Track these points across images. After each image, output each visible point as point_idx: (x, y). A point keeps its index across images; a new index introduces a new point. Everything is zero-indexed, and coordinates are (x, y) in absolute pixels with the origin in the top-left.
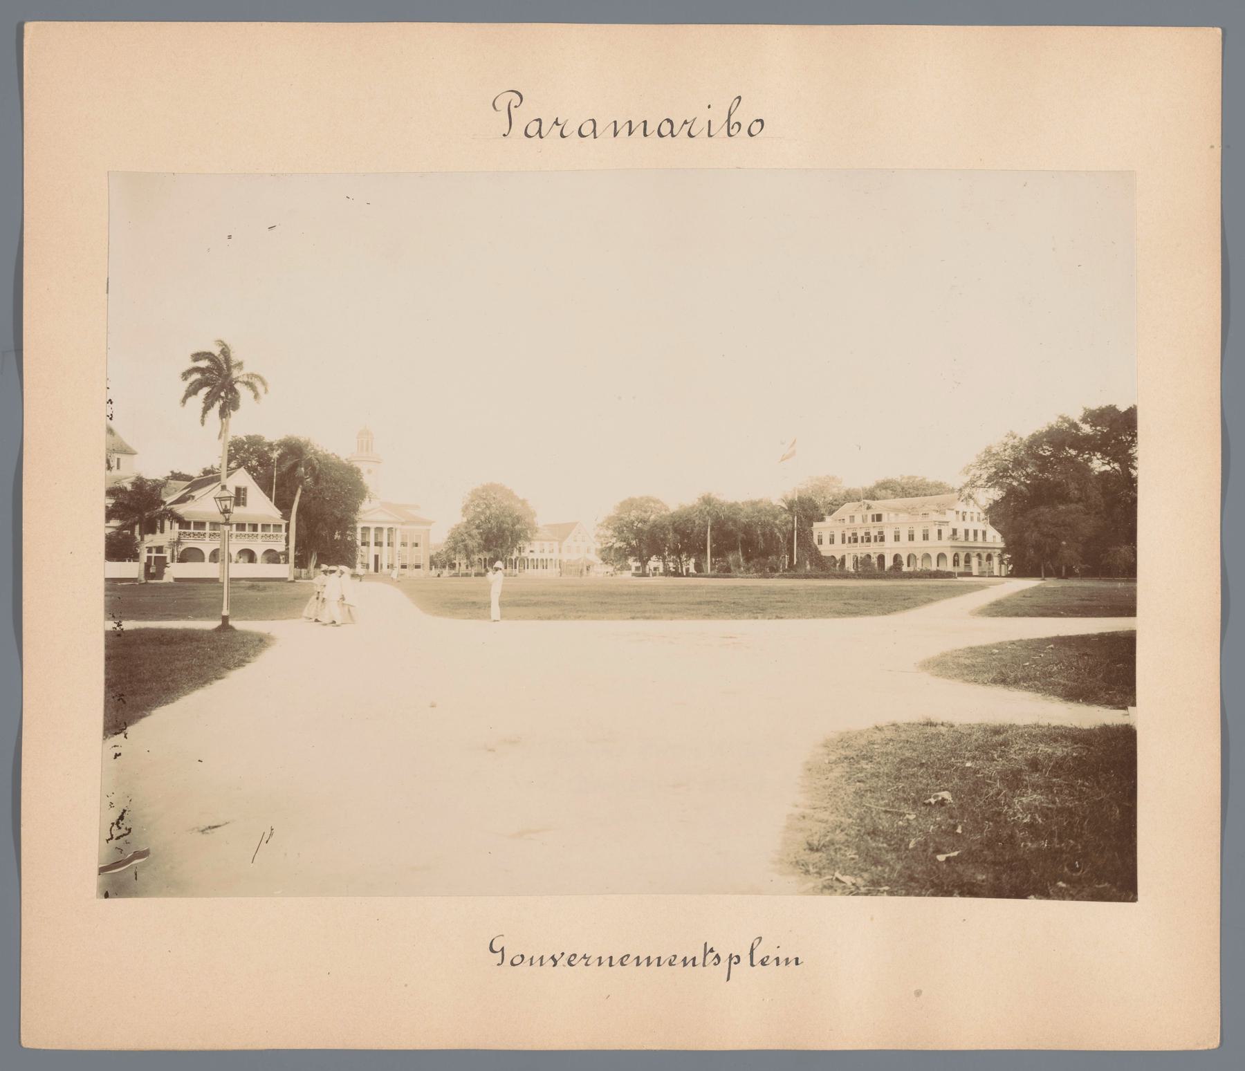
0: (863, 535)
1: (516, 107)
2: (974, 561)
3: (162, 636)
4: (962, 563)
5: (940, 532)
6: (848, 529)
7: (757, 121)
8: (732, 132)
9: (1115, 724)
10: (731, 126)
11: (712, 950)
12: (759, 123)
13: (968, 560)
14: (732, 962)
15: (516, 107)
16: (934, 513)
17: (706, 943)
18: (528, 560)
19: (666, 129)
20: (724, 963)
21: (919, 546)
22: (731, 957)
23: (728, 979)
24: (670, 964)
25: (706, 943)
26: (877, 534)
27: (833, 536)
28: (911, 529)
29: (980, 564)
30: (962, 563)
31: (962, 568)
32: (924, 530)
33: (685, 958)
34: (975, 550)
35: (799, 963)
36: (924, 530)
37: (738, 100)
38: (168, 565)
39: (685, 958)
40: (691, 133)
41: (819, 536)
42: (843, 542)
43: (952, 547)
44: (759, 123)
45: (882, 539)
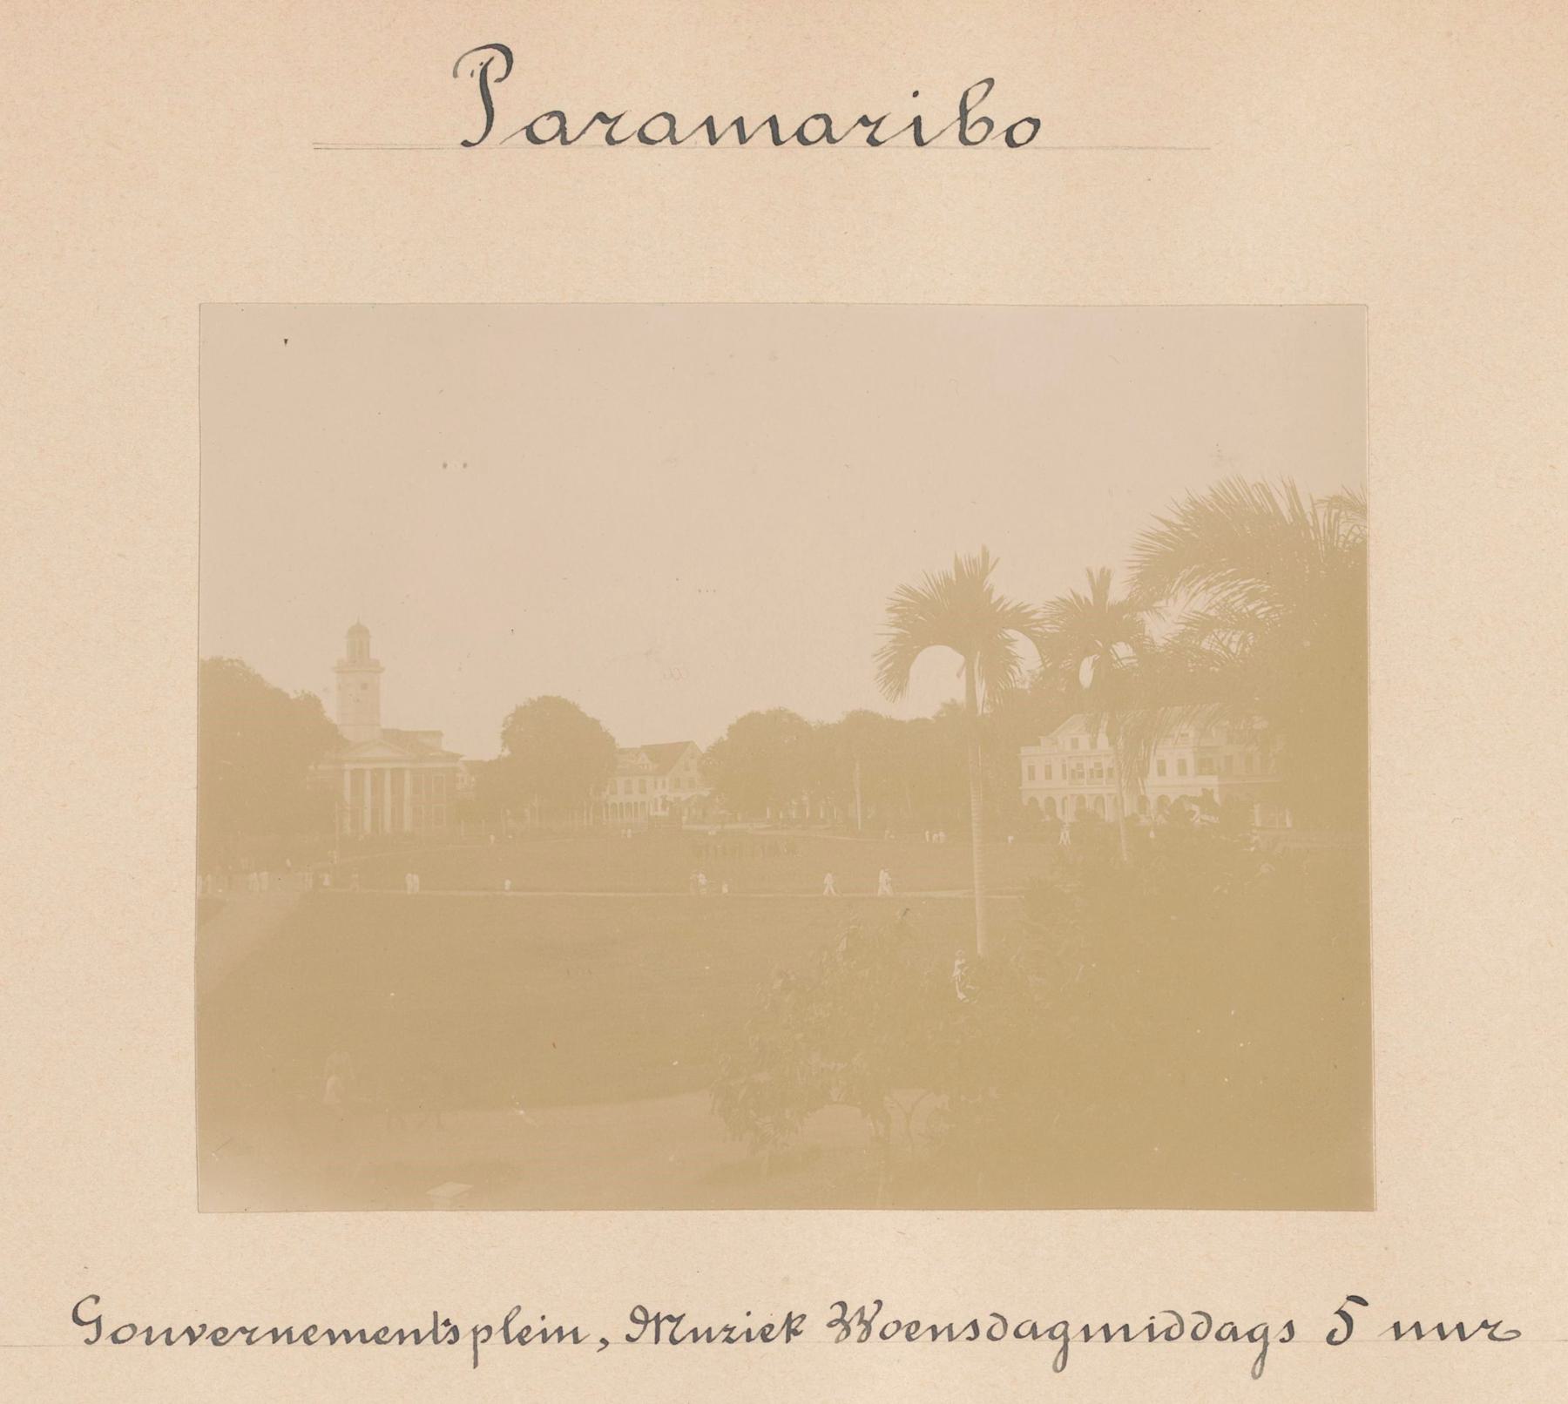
1: (499, 80)
6: (1070, 757)
7: (817, 117)
8: (971, 135)
10: (968, 125)
11: (447, 1323)
12: (822, 121)
14: (479, 1340)
15: (499, 80)
17: (1365, 1304)
18: (607, 805)
19: (814, 130)
20: (466, 1340)
22: (475, 1331)
23: (476, 1365)
24: (1168, 1338)
25: (1365, 1304)
26: (1092, 766)
27: (1050, 767)
33: (401, 1343)
35: (580, 1338)
36: (1179, 760)
37: (985, 86)
39: (401, 1343)
40: (613, 135)
42: (1064, 776)
44: (822, 121)
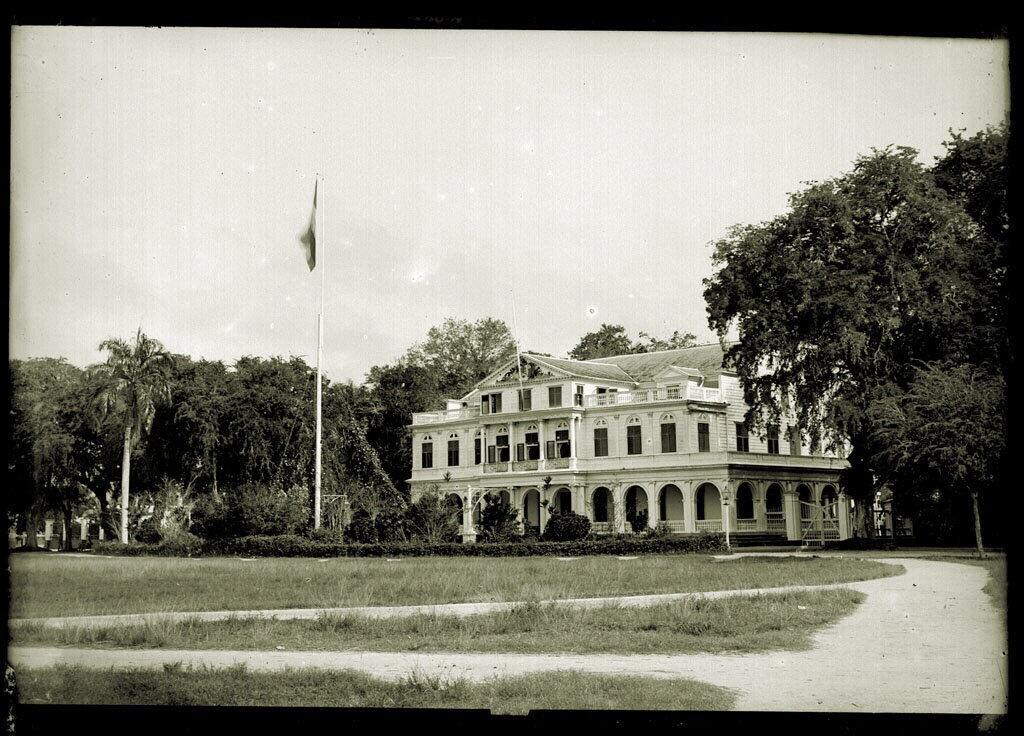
0: (523, 440)
2: (790, 504)
3: (40, 368)
4: (760, 508)
5: (703, 429)
9: (209, 667)
13: (774, 500)
16: (692, 384)
21: (651, 468)
28: (454, 439)
29: (804, 512)
30: (760, 508)
31: (759, 525)
32: (450, 443)
34: (623, 478)
36: (450, 443)
38: (827, 501)
41: (424, 445)
43: (731, 467)
45: (566, 452)
